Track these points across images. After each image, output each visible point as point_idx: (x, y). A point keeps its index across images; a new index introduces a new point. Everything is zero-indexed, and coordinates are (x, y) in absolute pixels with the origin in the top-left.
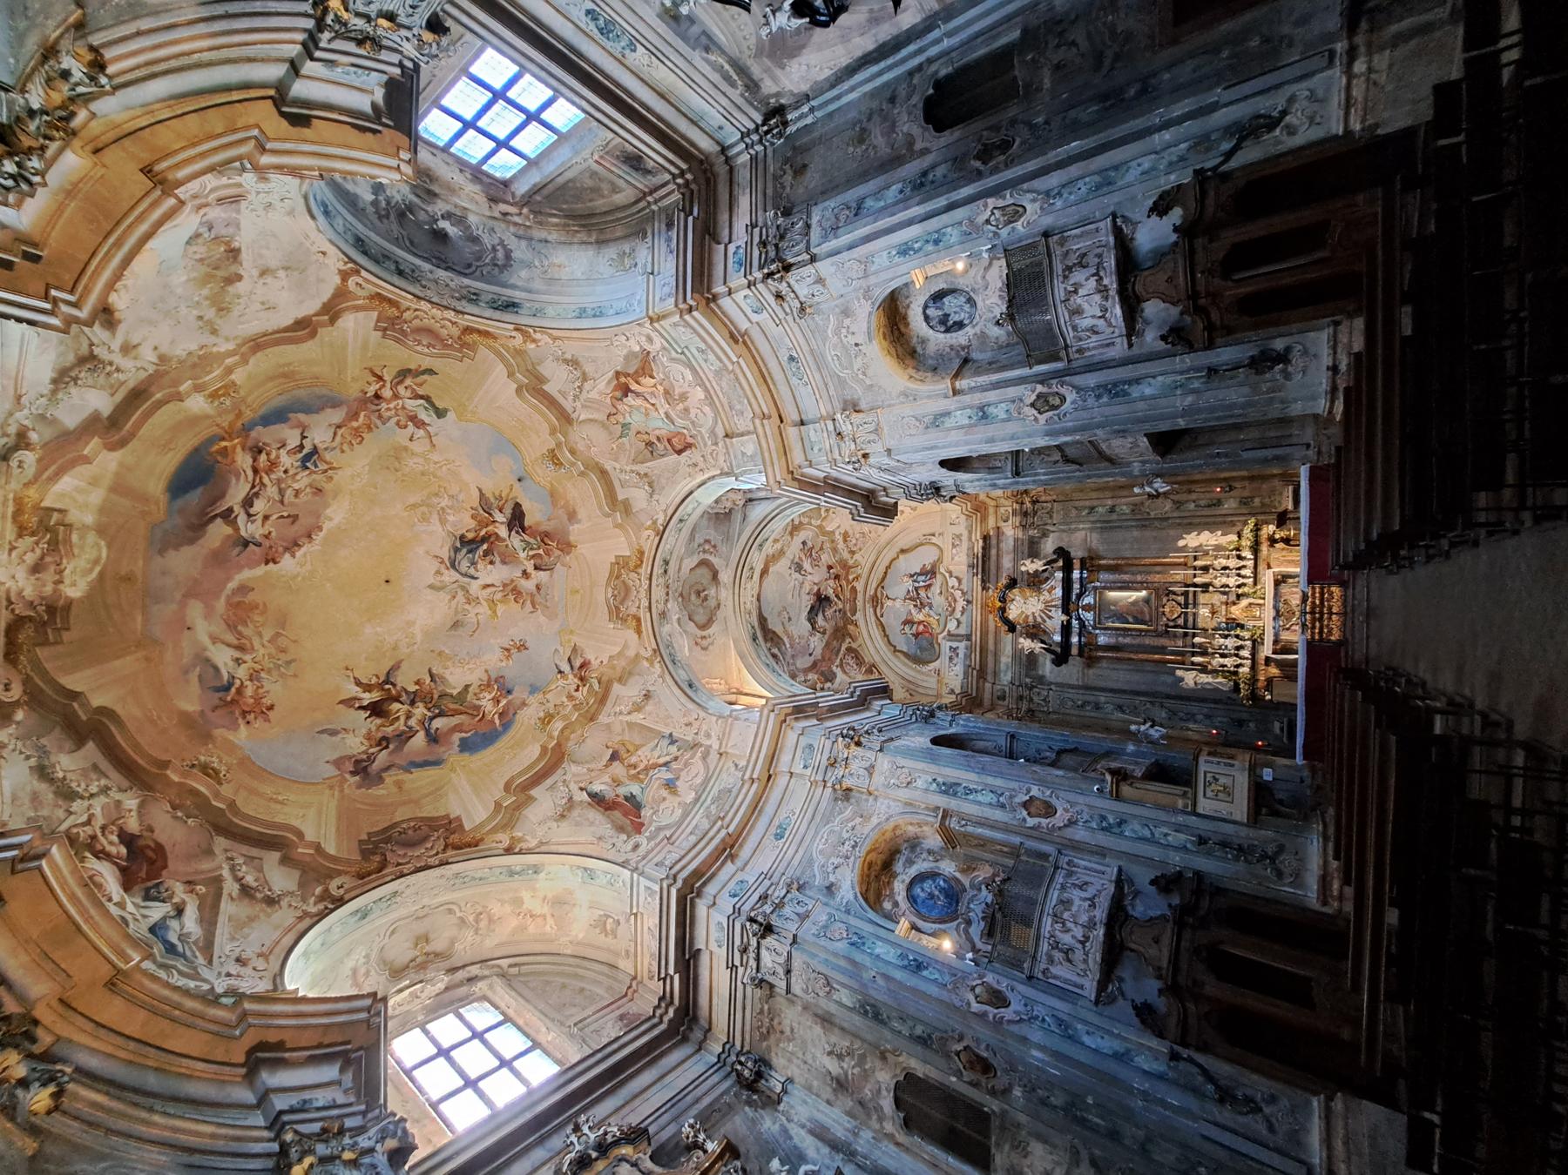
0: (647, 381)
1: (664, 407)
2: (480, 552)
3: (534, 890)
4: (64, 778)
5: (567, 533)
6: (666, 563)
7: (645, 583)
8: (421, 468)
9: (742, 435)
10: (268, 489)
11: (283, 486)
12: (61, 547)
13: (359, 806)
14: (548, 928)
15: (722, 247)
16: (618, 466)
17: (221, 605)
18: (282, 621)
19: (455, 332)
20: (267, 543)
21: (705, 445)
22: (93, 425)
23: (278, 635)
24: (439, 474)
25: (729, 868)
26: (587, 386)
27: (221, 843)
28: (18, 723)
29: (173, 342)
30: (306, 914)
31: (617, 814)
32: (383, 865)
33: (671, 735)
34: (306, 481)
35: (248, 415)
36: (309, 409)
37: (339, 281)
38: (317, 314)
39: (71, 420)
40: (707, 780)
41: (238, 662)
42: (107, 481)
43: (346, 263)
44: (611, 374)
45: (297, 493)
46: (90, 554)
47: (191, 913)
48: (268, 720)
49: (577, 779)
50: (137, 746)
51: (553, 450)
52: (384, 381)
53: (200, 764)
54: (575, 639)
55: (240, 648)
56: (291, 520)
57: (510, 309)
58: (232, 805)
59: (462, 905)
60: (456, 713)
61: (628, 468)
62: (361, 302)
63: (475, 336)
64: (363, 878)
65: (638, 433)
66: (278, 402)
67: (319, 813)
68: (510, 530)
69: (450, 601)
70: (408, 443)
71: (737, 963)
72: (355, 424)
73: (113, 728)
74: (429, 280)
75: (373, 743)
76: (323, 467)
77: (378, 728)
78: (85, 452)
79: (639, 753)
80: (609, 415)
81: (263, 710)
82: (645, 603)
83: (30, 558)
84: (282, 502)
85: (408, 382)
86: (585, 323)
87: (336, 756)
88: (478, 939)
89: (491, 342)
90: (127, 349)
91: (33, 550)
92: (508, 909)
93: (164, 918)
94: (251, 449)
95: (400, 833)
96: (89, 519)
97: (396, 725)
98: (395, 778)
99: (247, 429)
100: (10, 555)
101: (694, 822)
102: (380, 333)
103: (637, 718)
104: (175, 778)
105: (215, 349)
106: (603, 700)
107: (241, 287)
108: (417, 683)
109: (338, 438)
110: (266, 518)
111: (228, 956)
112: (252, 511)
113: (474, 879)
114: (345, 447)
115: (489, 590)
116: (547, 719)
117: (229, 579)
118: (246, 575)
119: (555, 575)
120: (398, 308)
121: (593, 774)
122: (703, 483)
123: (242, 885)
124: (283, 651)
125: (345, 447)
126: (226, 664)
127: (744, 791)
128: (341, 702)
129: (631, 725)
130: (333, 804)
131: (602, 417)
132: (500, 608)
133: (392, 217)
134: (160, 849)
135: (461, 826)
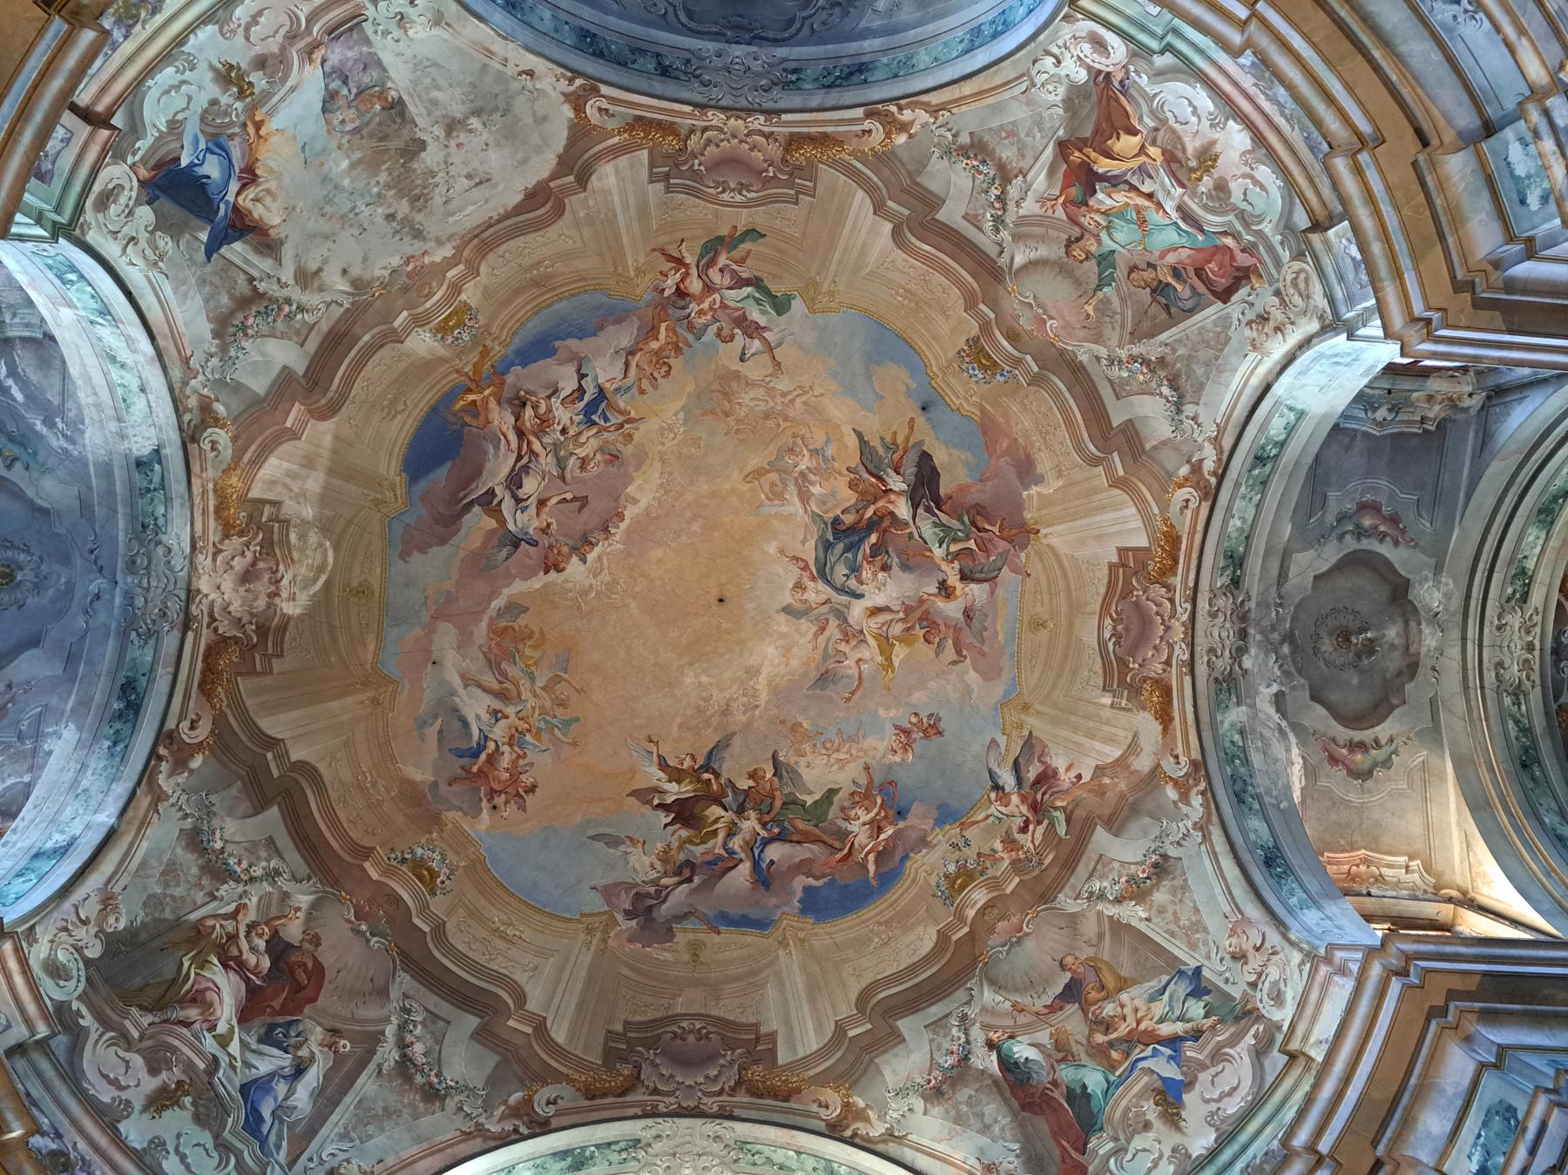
0: (1127, 143)
1: (1172, 196)
2: (866, 547)
4: (222, 850)
5: (1019, 506)
8: (763, 407)
10: (542, 459)
11: (562, 453)
12: (277, 550)
13: (625, 971)
17: (481, 631)
18: (565, 660)
19: (775, 151)
21: (1278, 264)
22: (285, 386)
23: (557, 679)
26: (1013, 191)
27: (404, 981)
28: (192, 772)
29: (365, 259)
30: (480, 1129)
31: (1042, 1125)
33: (1198, 970)
34: (594, 443)
36: (582, 332)
37: (571, 114)
38: (552, 178)
39: (259, 385)
41: (496, 715)
42: (324, 460)
43: (571, 81)
44: (1049, 153)
45: (584, 463)
46: (313, 559)
47: (313, 1077)
48: (522, 808)
49: (987, 1020)
50: (334, 823)
51: (976, 340)
52: (687, 266)
53: (414, 861)
54: (1031, 721)
55: (502, 695)
57: (855, 79)
58: (439, 929)
62: (616, 139)
63: (808, 151)
64: (593, 1098)
65: (1133, 268)
66: (535, 326)
68: (915, 506)
69: (816, 636)
70: (735, 365)
72: (654, 345)
73: (309, 793)
74: (717, 69)
76: (615, 419)
77: (684, 843)
78: (288, 424)
79: (1124, 997)
80: (1069, 244)
81: (518, 791)
82: (1181, 653)
83: (239, 564)
84: (562, 478)
85: (723, 260)
86: (981, 58)
87: (609, 880)
90: (305, 278)
91: (243, 554)
93: (272, 1076)
94: (510, 402)
96: (309, 512)
97: (710, 844)
98: (690, 936)
99: (500, 372)
100: (214, 560)
102: (660, 186)
103: (1133, 913)
104: (374, 875)
105: (427, 260)
106: (1070, 859)
107: (431, 157)
108: (752, 776)
109: (633, 371)
110: (542, 503)
111: (322, 1163)
112: (521, 493)
114: (645, 384)
115: (882, 618)
117: (494, 594)
118: (519, 587)
119: (1000, 592)
120: (676, 134)
121: (1022, 1019)
122: (1289, 360)
123: (404, 1056)
124: (563, 704)
125: (645, 384)
126: (478, 717)
128: (633, 793)
129: (1119, 928)
131: (1054, 251)
132: (900, 653)
134: (318, 971)
135: (772, 1052)
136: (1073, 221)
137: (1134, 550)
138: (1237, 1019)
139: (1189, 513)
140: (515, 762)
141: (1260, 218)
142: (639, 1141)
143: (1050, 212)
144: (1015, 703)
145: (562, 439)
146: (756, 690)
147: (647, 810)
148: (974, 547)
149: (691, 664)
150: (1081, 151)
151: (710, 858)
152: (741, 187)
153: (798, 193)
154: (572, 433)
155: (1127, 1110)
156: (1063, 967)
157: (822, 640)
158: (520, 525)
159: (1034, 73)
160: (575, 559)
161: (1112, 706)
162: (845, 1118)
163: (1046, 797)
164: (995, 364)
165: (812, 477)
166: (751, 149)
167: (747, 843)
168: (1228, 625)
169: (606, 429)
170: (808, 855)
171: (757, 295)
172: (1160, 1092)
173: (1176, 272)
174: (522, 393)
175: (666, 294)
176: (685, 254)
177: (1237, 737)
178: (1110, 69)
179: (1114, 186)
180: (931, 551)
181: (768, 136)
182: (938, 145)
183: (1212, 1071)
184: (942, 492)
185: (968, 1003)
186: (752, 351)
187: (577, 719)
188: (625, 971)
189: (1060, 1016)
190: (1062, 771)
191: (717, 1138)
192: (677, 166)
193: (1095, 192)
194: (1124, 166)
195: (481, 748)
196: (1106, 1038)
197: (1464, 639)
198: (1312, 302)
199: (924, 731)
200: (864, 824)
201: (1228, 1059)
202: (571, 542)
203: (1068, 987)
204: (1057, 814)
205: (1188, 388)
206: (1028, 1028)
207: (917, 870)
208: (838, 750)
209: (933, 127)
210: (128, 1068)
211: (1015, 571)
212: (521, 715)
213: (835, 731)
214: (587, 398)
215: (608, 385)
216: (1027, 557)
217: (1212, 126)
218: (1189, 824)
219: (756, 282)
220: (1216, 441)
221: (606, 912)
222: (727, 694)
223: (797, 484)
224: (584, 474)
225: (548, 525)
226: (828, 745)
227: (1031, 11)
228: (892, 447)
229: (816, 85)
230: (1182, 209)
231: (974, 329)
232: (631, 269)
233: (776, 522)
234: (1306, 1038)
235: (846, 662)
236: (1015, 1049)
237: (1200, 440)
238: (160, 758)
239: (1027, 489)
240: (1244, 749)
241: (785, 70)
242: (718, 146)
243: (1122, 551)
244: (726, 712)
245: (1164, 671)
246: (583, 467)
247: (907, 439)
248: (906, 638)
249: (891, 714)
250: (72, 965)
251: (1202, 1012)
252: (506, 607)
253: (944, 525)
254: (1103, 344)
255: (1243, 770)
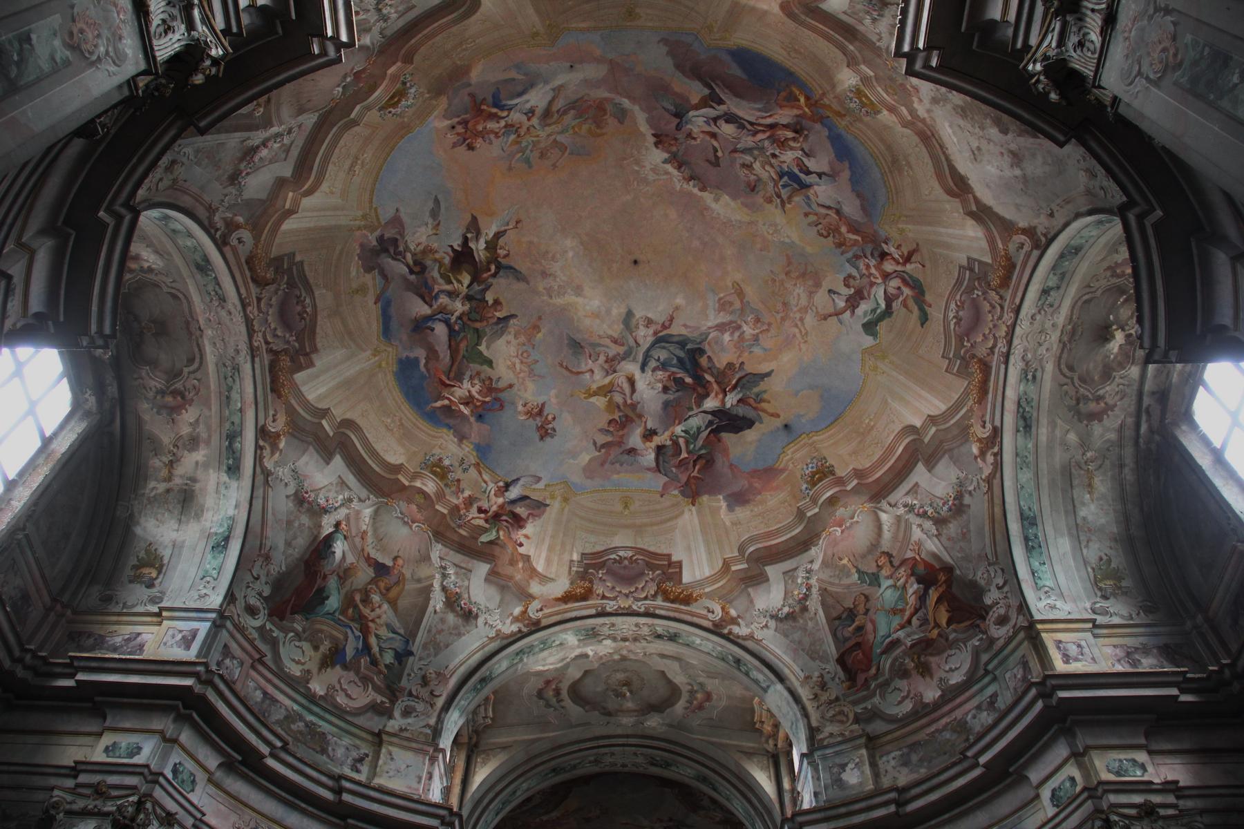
0: (943, 617)
1: (907, 637)
3: (206, 466)
5: (713, 491)
6: (673, 638)
7: (639, 606)
8: (793, 302)
9: (873, 765)
10: (750, 138)
13: (339, 248)
14: (152, 484)
15: (1143, 741)
16: (816, 566)
17: (603, 93)
19: (981, 351)
20: (680, 136)
21: (855, 703)
24: (787, 323)
25: (213, 762)
26: (928, 524)
32: (260, 282)
33: (411, 653)
34: (764, 176)
35: (842, 123)
38: (975, 198)
40: (340, 713)
43: (1045, 235)
44: (947, 558)
48: (455, 145)
51: (832, 473)
52: (904, 264)
54: (556, 505)
55: (547, 113)
56: (713, 159)
57: (1021, 423)
58: (355, 123)
59: (198, 375)
60: (453, 349)
61: (813, 581)
62: (1000, 246)
63: (978, 376)
64: (247, 263)
67: (335, 208)
68: (713, 413)
69: (610, 337)
70: (826, 285)
71: (83, 778)
72: (844, 229)
74: (1043, 324)
75: (419, 256)
76: (785, 193)
77: (441, 264)
79: (386, 606)
80: (889, 555)
82: (611, 606)
84: (735, 151)
85: (907, 291)
87: (406, 219)
88: (151, 395)
89: (974, 395)
92: (185, 430)
94: (798, 123)
95: (298, 297)
97: (441, 281)
98: (370, 283)
101: (281, 697)
102: (965, 263)
104: (391, 71)
105: (915, 99)
108: (497, 302)
109: (823, 211)
110: (714, 135)
112: (721, 123)
113: (230, 389)
114: (812, 218)
116: (439, 470)
119: (649, 475)
121: (358, 540)
123: (258, 147)
125: (812, 218)
126: (528, 101)
127: (324, 779)
128: (474, 219)
130: (343, 221)
132: (600, 402)
133: (1115, 280)
135: (300, 368)
136: (903, 562)
137: (681, 572)
138: (388, 687)
139: (704, 612)
140: (492, 131)
141: (883, 696)
142: (225, 301)
143: (911, 547)
144: (569, 492)
145: (768, 154)
146: (564, 295)
147: (461, 231)
148: (682, 457)
149: (582, 243)
150: (945, 582)
151: (430, 281)
152: (959, 321)
153: (950, 360)
154: (773, 161)
155: (321, 631)
156: (395, 559)
157: (608, 342)
158: (694, 119)
159: (996, 567)
160: (666, 155)
161: (572, 561)
162: (270, 437)
163: (505, 523)
164: (814, 484)
165: (737, 334)
166: (984, 335)
167: (445, 308)
168: (631, 632)
169: (776, 185)
170: (441, 355)
171: (879, 311)
172: (337, 649)
173: (860, 628)
174: (806, 133)
175: (884, 246)
176: (913, 266)
177: (557, 643)
178: (987, 622)
179: (920, 598)
180: (679, 424)
181: (992, 349)
182: (966, 478)
183: (357, 680)
184: (724, 435)
185: (360, 500)
186: (837, 301)
187: (530, 167)
188: (339, 248)
189: (363, 564)
190: (524, 531)
191: (237, 352)
192: (979, 279)
193: (919, 583)
194: (931, 609)
195: (502, 108)
196: (358, 602)
197: (627, 736)
198: (828, 724)
199: (542, 427)
200: (469, 392)
201: (365, 688)
202: (680, 153)
203: (383, 565)
204: (494, 533)
205: (786, 626)
206: (353, 547)
207: (441, 437)
208: (522, 362)
209: (978, 477)
210: (899, 689)
211: (665, 486)
212: (532, 129)
213: (536, 358)
214: (802, 176)
215: (812, 191)
216: (675, 496)
217: (941, 679)
218: (499, 627)
219: (888, 312)
220: (751, 637)
221: (379, 223)
222: (559, 273)
223: (731, 322)
224: (738, 166)
225: (694, 139)
226: (525, 355)
227: (1033, 574)
228: (759, 399)
229: (1021, 393)
230: (896, 643)
231: (841, 472)
232: (904, 226)
233: (700, 304)
234: (391, 744)
235: (590, 362)
236: (338, 543)
237: (752, 626)
238: (262, 448)
239: (724, 498)
240: (550, 647)
241: (1036, 370)
242: (990, 312)
243: (679, 564)
244: (545, 274)
245: (598, 595)
246: (744, 165)
247: (764, 411)
248: (612, 405)
249: (551, 398)
250: (258, 603)
251: (387, 662)
252: (622, 109)
253: (699, 434)
254: (821, 568)
255: (537, 649)
